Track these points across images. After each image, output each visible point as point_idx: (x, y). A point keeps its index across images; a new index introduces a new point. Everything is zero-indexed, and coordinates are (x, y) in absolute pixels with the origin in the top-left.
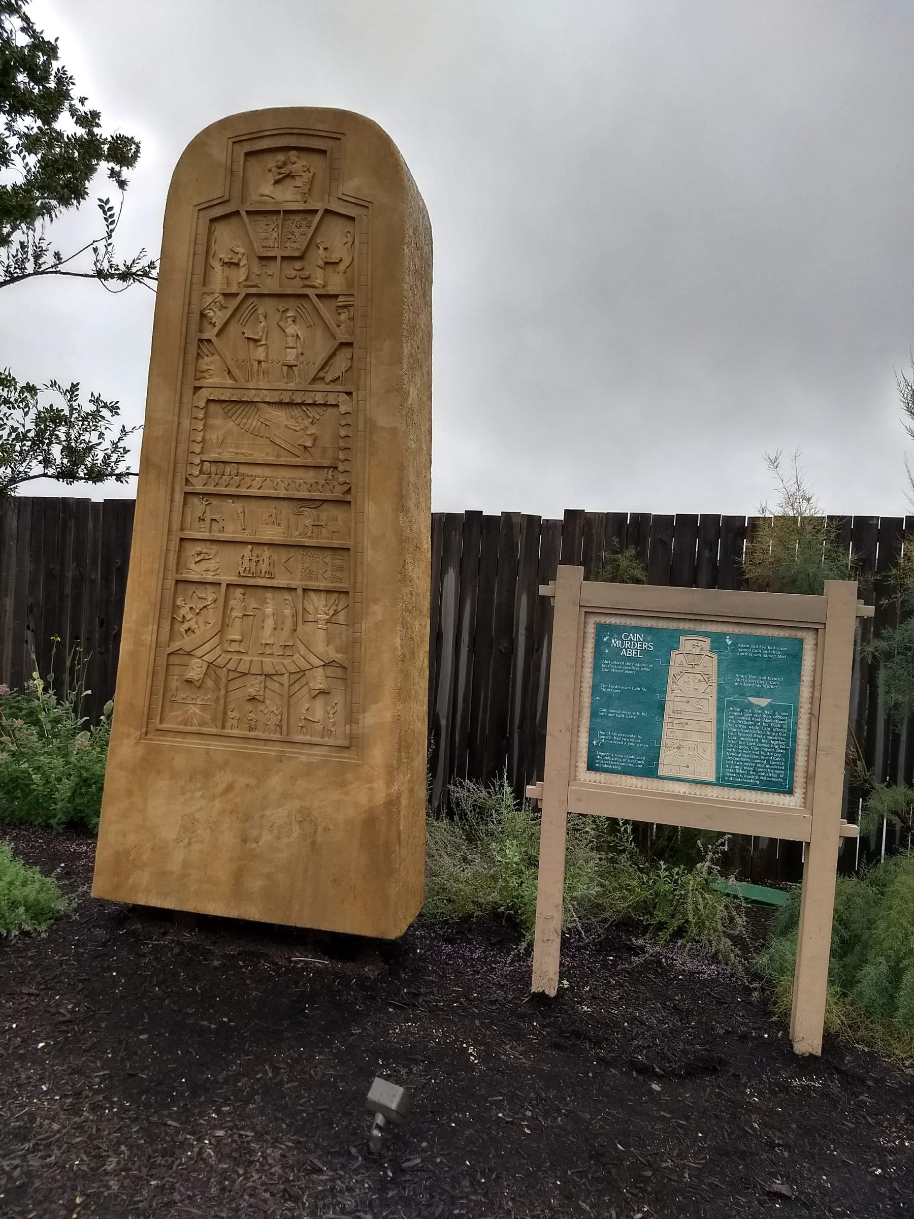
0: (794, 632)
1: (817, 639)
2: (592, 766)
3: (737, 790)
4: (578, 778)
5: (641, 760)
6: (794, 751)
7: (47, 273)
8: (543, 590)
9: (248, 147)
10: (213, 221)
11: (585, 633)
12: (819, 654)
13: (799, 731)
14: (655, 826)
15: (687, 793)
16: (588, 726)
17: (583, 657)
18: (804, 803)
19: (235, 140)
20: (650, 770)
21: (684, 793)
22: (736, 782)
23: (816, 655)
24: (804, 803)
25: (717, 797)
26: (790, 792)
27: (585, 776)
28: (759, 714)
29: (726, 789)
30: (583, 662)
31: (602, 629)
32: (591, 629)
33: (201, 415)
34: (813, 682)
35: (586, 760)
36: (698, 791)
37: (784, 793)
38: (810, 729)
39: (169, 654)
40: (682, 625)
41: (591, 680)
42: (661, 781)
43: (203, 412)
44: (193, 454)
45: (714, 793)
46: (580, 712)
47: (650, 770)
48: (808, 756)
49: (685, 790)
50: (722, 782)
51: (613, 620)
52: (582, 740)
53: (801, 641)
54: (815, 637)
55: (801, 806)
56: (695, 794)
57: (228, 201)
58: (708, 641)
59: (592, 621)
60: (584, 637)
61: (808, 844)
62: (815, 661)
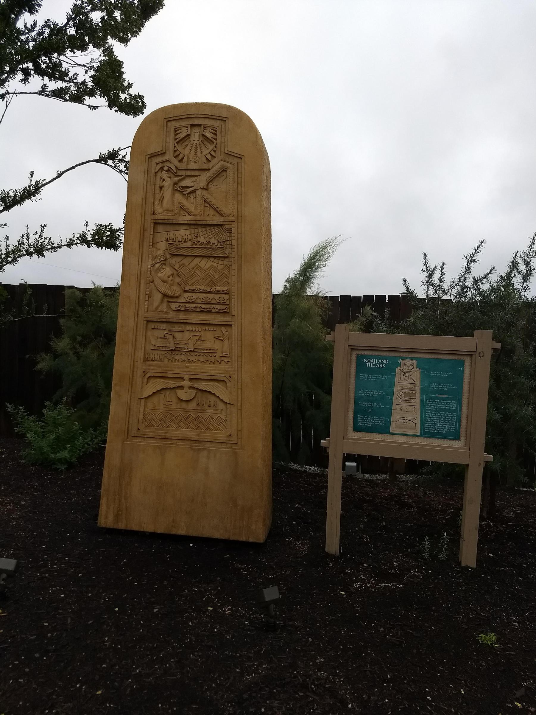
1: (471, 360)
2: (356, 429)
6: (460, 419)
7: (77, 63)
13: (463, 408)
14: (313, 469)
16: (353, 408)
18: (465, 444)
23: (471, 368)
24: (465, 444)
26: (458, 439)
28: (366, 418)
29: (425, 439)
31: (359, 358)
32: (354, 358)
35: (352, 426)
36: (411, 440)
37: (456, 440)
41: (354, 384)
45: (419, 441)
47: (385, 430)
48: (467, 420)
50: (424, 434)
51: (366, 353)
54: (471, 359)
55: (464, 446)
58: (415, 363)
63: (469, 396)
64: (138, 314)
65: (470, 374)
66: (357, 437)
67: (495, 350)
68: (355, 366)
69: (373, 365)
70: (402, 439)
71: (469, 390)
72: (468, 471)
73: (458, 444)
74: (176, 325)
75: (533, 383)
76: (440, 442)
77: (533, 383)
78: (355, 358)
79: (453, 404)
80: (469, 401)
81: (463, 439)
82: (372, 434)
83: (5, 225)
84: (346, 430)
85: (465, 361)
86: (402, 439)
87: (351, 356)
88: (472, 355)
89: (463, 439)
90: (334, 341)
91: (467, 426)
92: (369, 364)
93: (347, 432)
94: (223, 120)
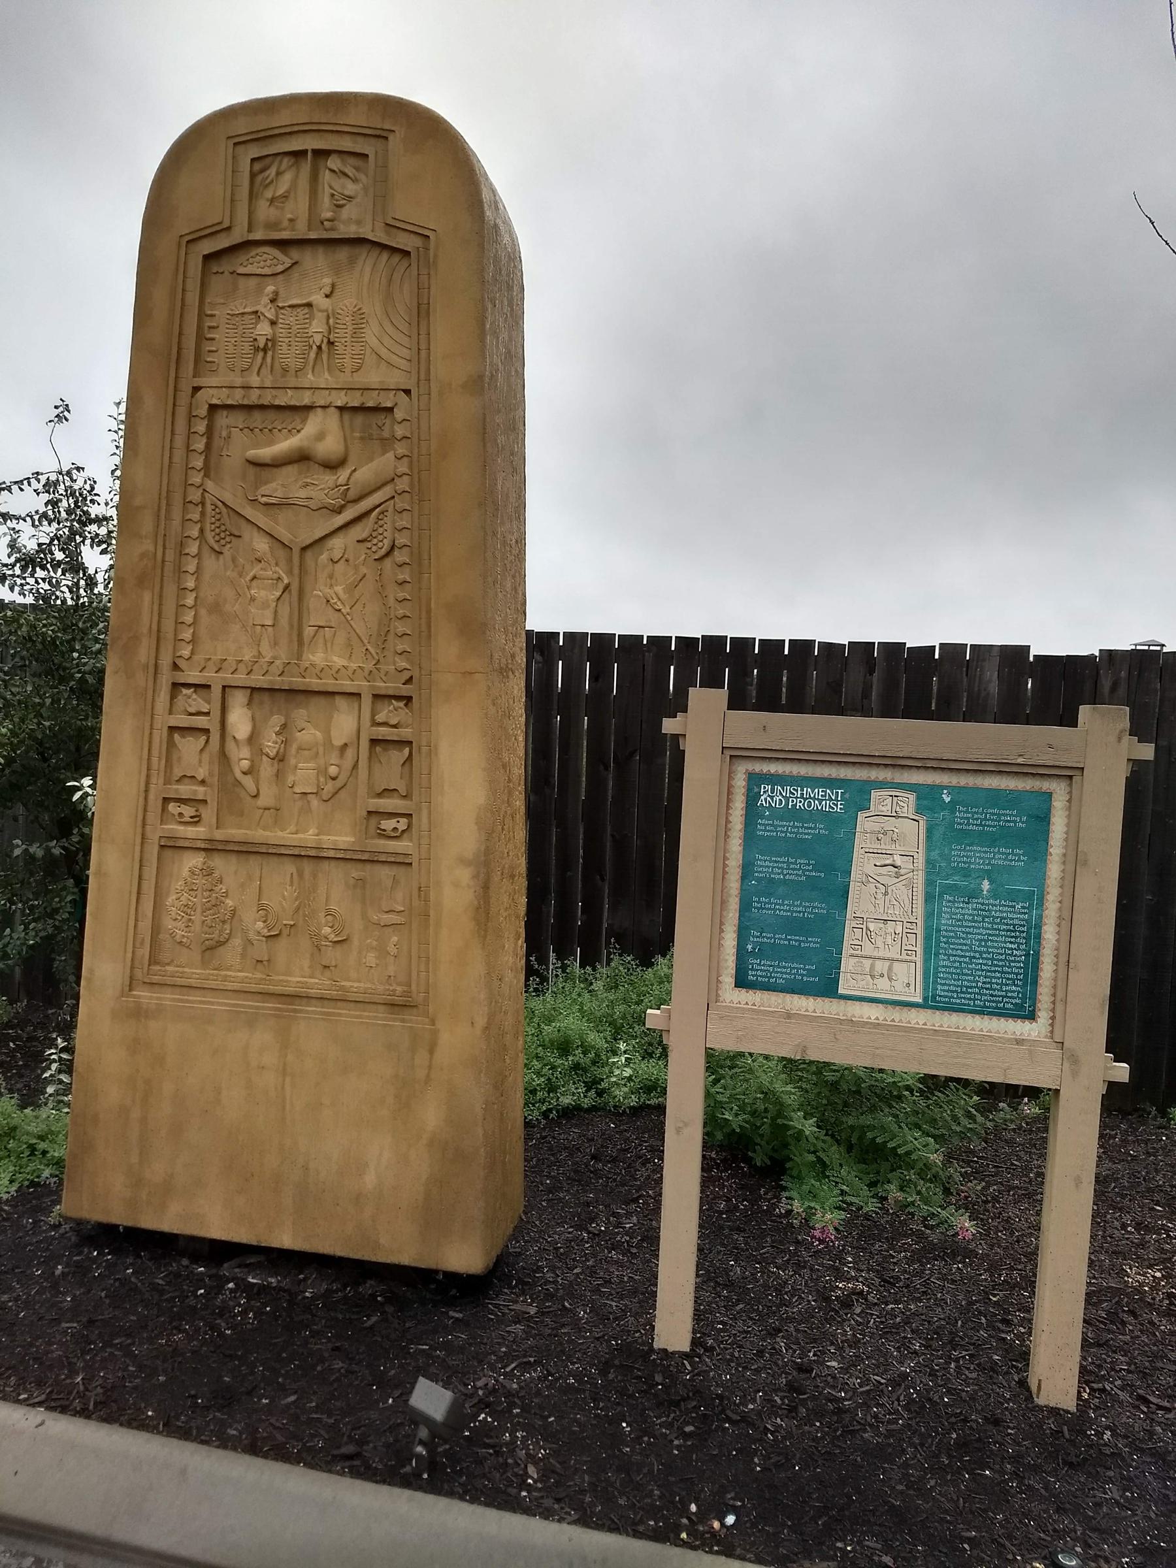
1: (1070, 793)
2: (741, 982)
11: (730, 787)
15: (881, 1018)
20: (828, 988)
21: (877, 1019)
25: (925, 1024)
26: (1032, 1016)
27: (732, 996)
32: (740, 782)
42: (842, 1002)
47: (828, 988)
50: (930, 1003)
54: (1068, 789)
55: (1046, 1037)
59: (742, 770)
64: (184, 290)
66: (747, 1004)
68: (744, 805)
70: (872, 1013)
72: (1057, 1110)
74: (238, 989)
75: (1174, 1368)
77: (1174, 1368)
79: (1013, 940)
82: (788, 995)
85: (1054, 795)
86: (872, 1013)
87: (730, 778)
88: (1070, 777)
89: (1043, 1016)
90: (1083, 768)
91: (1055, 979)
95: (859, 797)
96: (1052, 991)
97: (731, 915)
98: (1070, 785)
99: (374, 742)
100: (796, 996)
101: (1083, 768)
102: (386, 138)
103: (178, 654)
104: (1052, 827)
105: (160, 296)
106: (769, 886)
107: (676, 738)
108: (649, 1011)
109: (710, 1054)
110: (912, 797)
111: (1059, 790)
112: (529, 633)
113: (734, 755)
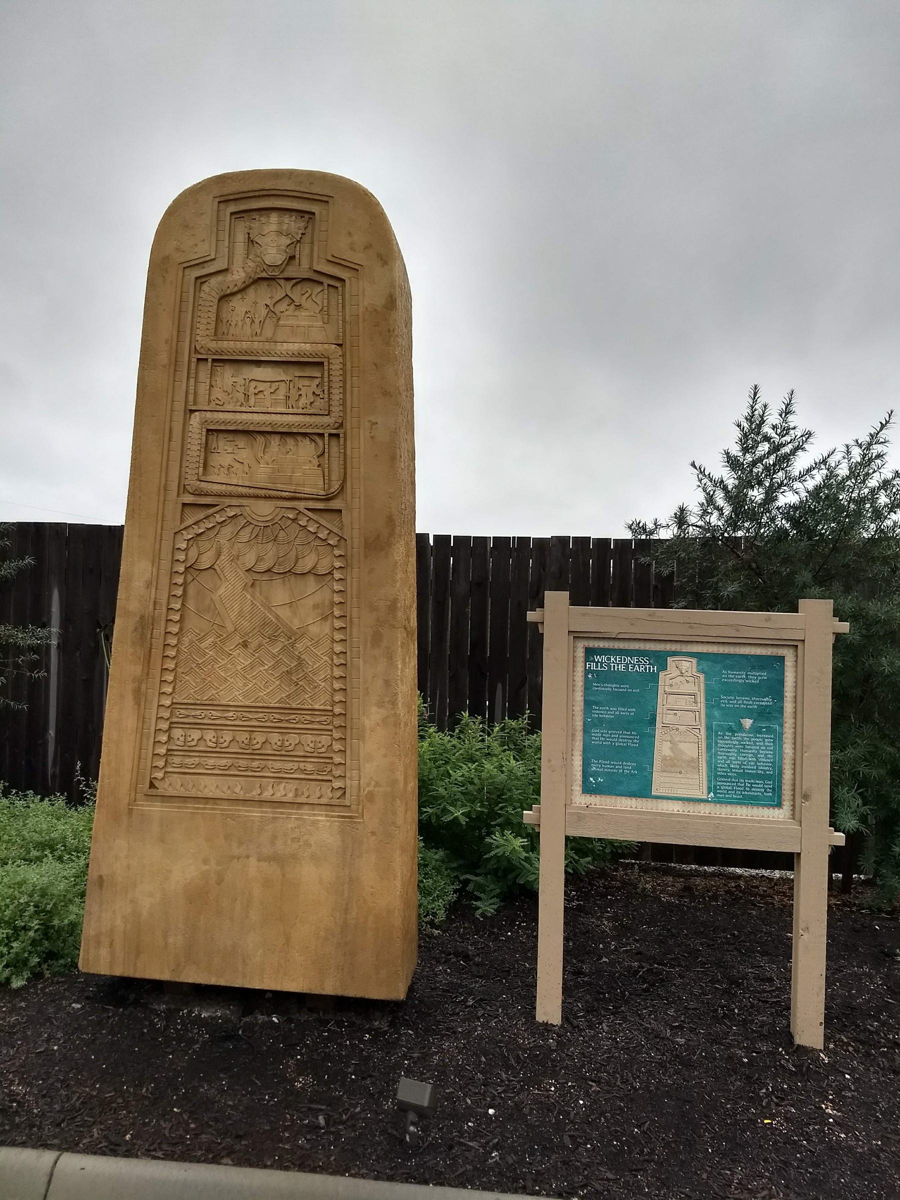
0: (775, 650)
1: (797, 656)
2: (587, 789)
3: (729, 806)
4: (573, 802)
5: (597, 733)
8: (531, 616)
9: (232, 208)
10: (184, 268)
11: (574, 657)
12: (800, 666)
15: (681, 810)
17: (574, 681)
19: (223, 199)
20: (644, 791)
21: (678, 811)
22: (728, 798)
23: (796, 672)
25: (710, 813)
26: (779, 805)
27: (581, 799)
30: (574, 686)
32: (336, 409)
33: (178, 606)
34: (795, 697)
37: (774, 806)
38: (795, 743)
39: (175, 533)
40: (669, 647)
42: (655, 800)
43: (178, 626)
44: (176, 586)
45: (704, 810)
46: (573, 735)
47: (644, 791)
49: (678, 808)
50: (717, 801)
52: (576, 763)
53: (782, 659)
54: (795, 653)
56: (689, 812)
57: (214, 259)
59: (581, 645)
60: (574, 661)
61: (799, 854)
62: (796, 677)
63: (795, 723)
65: (796, 682)
67: (838, 637)
69: (622, 668)
70: (675, 807)
71: (795, 713)
73: (779, 815)
76: (723, 809)
78: (583, 655)
80: (795, 733)
81: (787, 805)
83: (693, 465)
84: (569, 792)
86: (675, 807)
87: (574, 651)
89: (787, 805)
90: (804, 640)
92: (614, 666)
93: (572, 794)
94: (324, 201)
95: (660, 660)
96: (792, 787)
97: (578, 744)
98: (796, 651)
99: (208, 430)
100: (623, 798)
101: (804, 640)
102: (328, 202)
103: (176, 558)
104: (786, 679)
105: (166, 328)
106: (600, 723)
107: (535, 625)
108: (524, 812)
109: (567, 838)
110: (694, 661)
111: (788, 655)
112: (422, 539)
113: (576, 635)
